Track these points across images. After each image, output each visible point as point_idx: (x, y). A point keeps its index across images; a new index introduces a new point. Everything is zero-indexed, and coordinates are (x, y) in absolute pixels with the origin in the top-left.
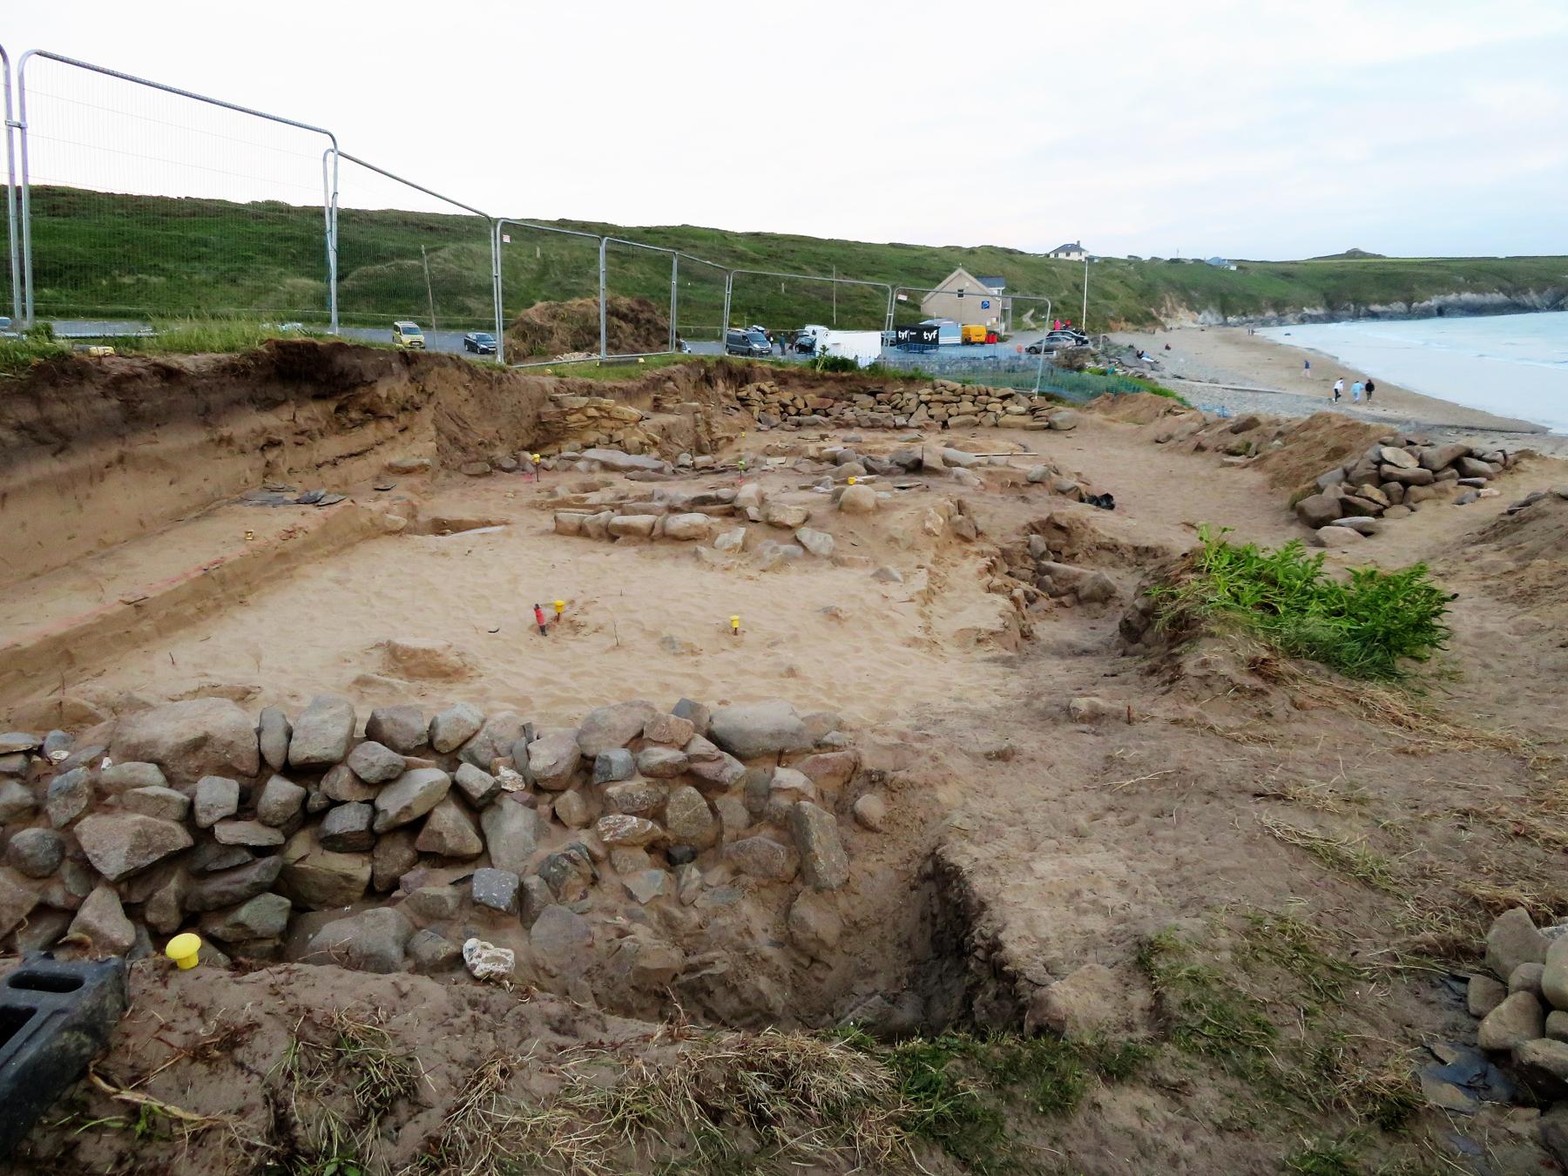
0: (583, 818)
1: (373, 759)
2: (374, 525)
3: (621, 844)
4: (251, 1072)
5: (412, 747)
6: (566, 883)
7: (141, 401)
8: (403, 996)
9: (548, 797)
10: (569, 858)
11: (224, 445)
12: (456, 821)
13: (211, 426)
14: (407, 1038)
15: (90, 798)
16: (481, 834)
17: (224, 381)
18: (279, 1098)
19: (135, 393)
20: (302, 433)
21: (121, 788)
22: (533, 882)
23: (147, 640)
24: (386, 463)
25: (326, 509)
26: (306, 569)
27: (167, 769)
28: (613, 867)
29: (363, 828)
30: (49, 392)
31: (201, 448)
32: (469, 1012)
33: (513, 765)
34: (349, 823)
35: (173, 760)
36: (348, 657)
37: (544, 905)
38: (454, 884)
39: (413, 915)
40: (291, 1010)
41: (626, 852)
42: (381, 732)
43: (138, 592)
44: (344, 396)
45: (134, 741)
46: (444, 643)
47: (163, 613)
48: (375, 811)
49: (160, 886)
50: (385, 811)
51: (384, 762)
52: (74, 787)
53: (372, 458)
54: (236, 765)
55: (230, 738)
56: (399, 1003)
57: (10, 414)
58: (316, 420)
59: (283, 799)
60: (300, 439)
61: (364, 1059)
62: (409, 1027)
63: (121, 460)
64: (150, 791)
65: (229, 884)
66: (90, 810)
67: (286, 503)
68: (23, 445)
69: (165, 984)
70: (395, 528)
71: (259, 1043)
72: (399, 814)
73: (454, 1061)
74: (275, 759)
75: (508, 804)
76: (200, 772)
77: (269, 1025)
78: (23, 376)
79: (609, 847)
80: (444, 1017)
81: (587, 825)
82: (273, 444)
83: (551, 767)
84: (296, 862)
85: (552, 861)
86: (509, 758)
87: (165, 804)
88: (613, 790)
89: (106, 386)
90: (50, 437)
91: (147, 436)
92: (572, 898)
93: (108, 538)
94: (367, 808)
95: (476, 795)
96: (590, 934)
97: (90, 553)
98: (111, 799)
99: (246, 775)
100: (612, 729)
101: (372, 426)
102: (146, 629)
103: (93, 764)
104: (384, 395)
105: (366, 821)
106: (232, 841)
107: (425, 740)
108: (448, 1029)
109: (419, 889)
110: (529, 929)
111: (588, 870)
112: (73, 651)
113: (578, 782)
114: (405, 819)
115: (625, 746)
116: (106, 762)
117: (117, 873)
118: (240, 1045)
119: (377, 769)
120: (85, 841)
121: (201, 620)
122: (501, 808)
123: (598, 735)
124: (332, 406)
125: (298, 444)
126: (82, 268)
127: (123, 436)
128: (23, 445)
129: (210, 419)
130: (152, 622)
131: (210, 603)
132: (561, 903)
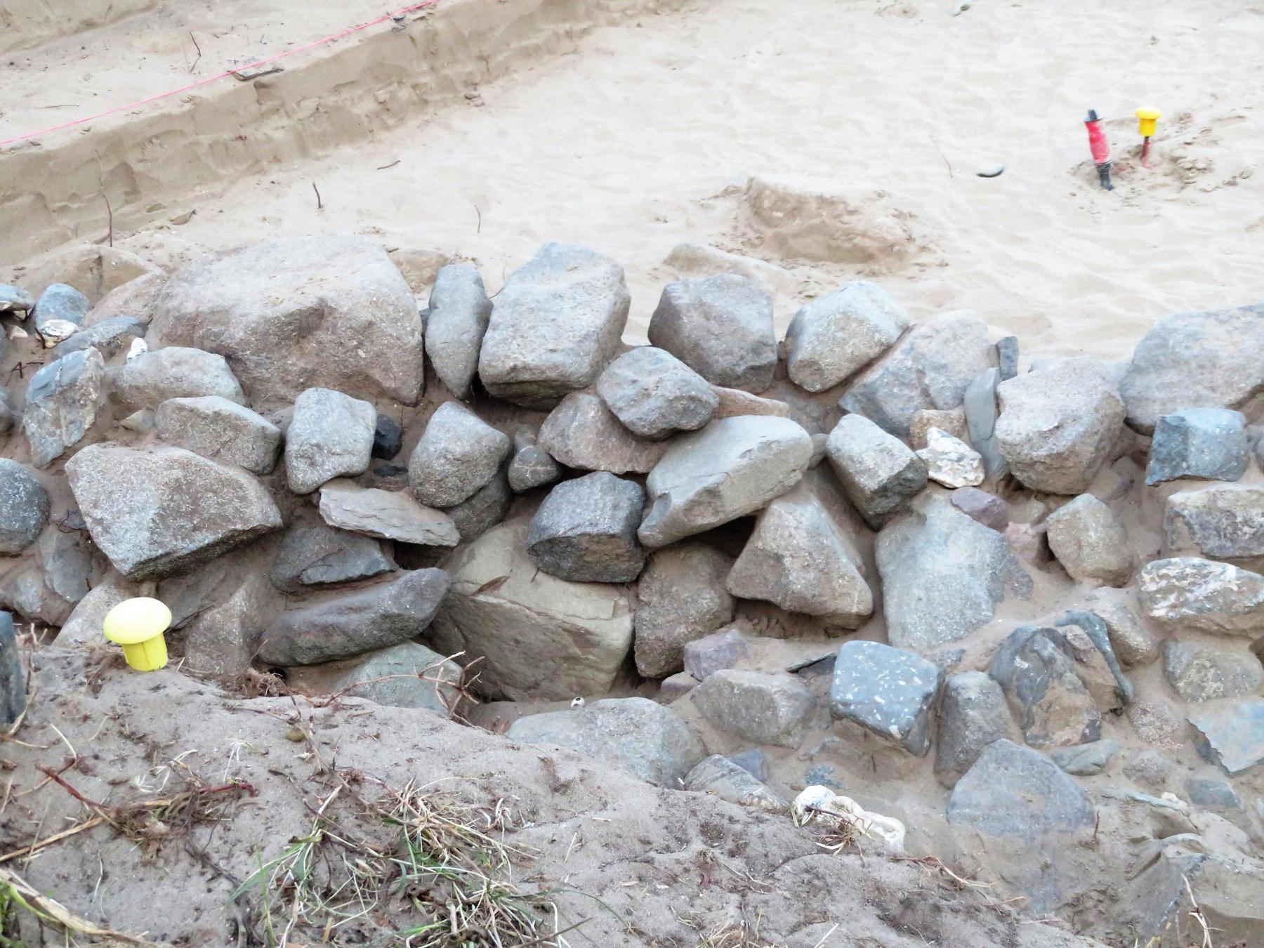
0: (1112, 562)
1: (649, 381)
3: (1192, 627)
4: (218, 874)
5: (740, 369)
6: (1049, 695)
8: (560, 788)
9: (1036, 507)
10: (1063, 643)
12: (814, 533)
14: (548, 872)
15: (100, 412)
16: (874, 576)
18: (259, 930)
21: (155, 396)
22: (971, 683)
23: (277, 159)
27: (246, 370)
28: (1170, 680)
29: (617, 528)
32: (698, 845)
33: (963, 429)
34: (588, 516)
35: (257, 352)
37: (989, 740)
38: (795, 671)
39: (703, 726)
40: (321, 773)
41: (1209, 648)
42: (677, 332)
43: (267, 58)
45: (189, 308)
46: (870, 187)
47: (310, 104)
48: (647, 499)
49: (213, 601)
50: (664, 497)
51: (669, 390)
52: (72, 385)
54: (377, 374)
55: (365, 316)
56: (546, 800)
59: (458, 449)
61: (444, 888)
62: (556, 849)
64: (205, 404)
65: (341, 612)
66: (98, 435)
69: (95, 690)
71: (246, 823)
72: (692, 505)
73: (640, 933)
74: (453, 370)
75: (939, 512)
76: (308, 380)
77: (271, 793)
79: (1165, 631)
80: (638, 847)
81: (1119, 578)
83: (1044, 436)
84: (481, 590)
85: (1021, 644)
86: (956, 413)
87: (230, 434)
88: (1187, 499)
92: (1061, 735)
94: (631, 490)
95: (869, 483)
96: (1094, 820)
98: (136, 417)
99: (395, 398)
100: (1209, 363)
102: (278, 135)
103: (113, 349)
105: (622, 514)
106: (351, 523)
107: (770, 357)
108: (642, 868)
109: (721, 673)
110: (950, 788)
111: (1105, 677)
112: (138, 167)
113: (1112, 479)
114: (707, 519)
115: (1238, 406)
116: (138, 345)
117: (134, 558)
118: (209, 821)
119: (654, 403)
120: (82, 492)
121: (387, 128)
122: (922, 519)
123: (1171, 376)
130: (285, 122)
131: (405, 94)
132: (1033, 743)
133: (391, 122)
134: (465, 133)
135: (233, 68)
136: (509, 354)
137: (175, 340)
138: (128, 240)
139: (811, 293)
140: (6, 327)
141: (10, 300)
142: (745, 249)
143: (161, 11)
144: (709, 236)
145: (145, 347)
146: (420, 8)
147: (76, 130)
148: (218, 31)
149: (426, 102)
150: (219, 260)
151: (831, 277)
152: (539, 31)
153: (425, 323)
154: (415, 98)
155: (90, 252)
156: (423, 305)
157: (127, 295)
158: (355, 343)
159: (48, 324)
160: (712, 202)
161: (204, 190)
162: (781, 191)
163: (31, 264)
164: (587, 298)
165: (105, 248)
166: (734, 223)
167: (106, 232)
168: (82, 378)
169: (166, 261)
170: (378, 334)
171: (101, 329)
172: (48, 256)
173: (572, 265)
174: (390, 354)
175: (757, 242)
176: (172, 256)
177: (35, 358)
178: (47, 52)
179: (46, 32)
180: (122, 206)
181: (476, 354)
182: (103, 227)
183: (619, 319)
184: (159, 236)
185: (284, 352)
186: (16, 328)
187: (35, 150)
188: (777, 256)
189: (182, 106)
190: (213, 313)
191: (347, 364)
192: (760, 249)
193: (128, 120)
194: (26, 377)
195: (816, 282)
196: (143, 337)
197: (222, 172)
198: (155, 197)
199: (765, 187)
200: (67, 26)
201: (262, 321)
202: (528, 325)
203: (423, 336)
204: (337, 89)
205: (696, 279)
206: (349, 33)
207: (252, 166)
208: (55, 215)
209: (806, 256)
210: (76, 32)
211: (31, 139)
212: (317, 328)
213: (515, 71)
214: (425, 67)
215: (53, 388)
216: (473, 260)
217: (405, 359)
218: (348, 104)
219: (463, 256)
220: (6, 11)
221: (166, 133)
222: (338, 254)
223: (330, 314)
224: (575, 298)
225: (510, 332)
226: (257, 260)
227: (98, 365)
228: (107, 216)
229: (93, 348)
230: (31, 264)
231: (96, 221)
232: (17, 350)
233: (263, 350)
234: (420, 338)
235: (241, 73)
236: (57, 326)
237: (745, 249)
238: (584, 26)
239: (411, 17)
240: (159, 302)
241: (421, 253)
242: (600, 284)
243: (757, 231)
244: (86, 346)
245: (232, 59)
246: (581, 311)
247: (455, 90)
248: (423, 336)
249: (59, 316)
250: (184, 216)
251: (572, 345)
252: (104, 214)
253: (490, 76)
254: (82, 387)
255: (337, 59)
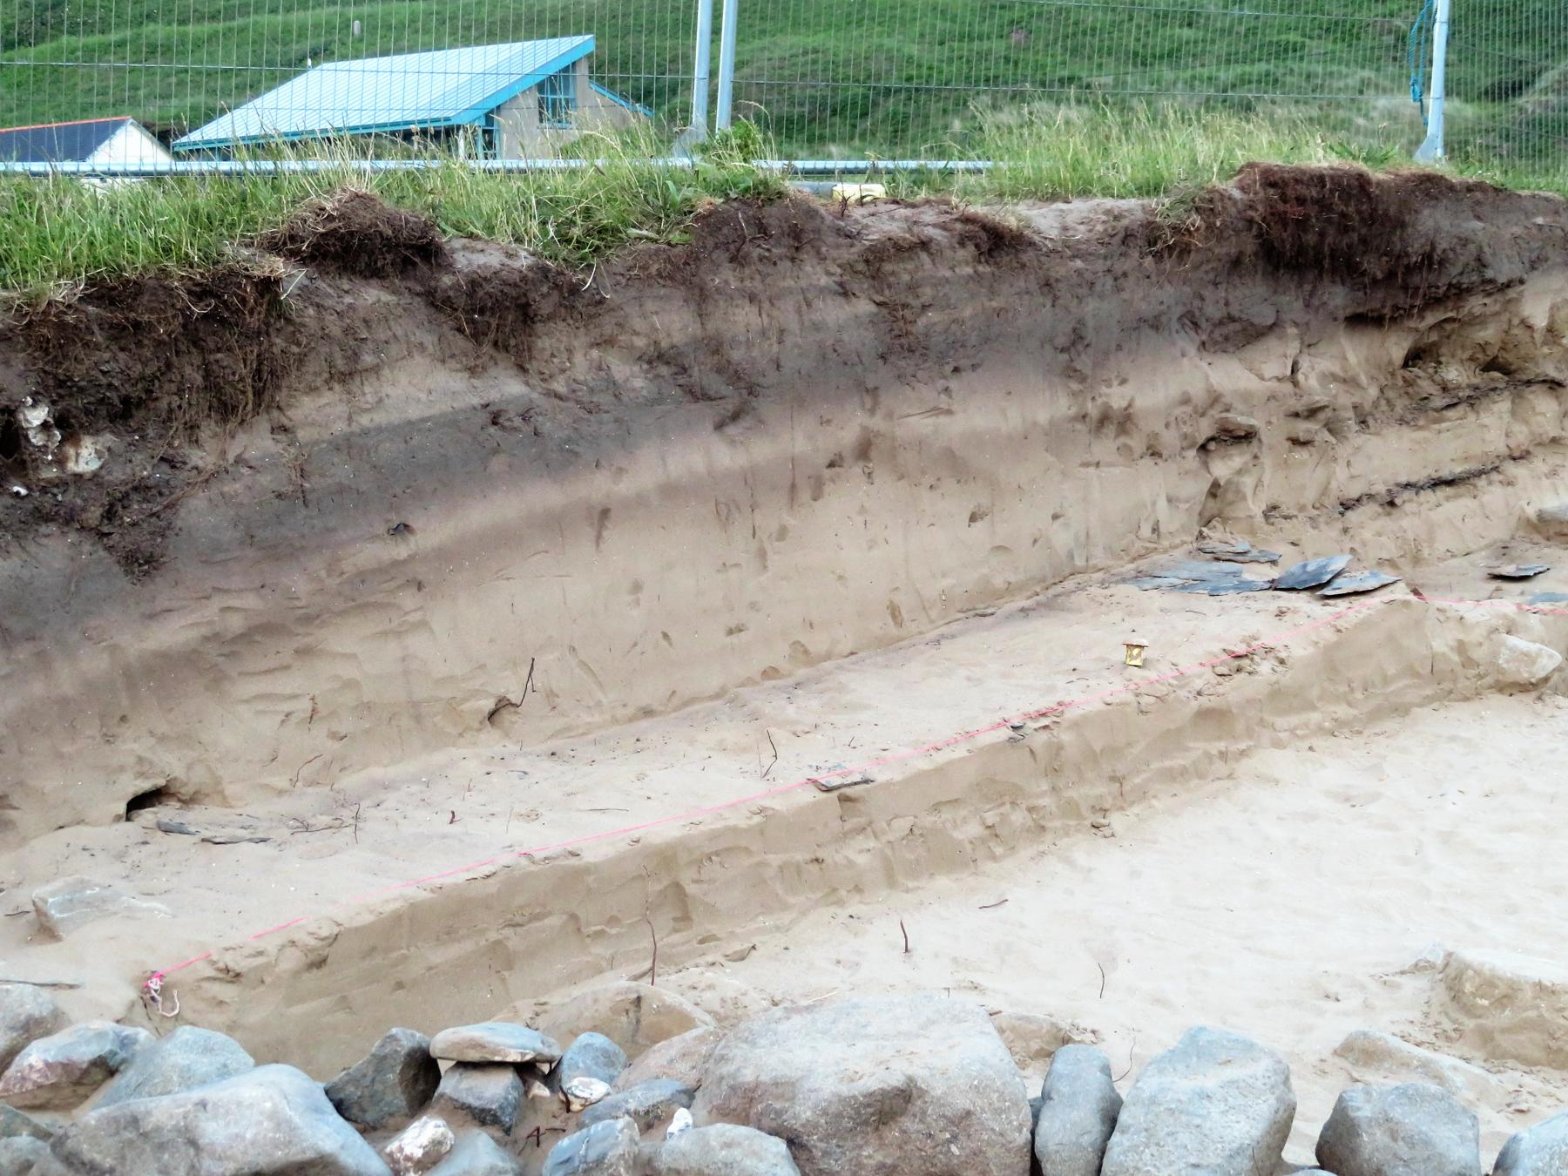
2: (1468, 662)
7: (925, 307)
11: (1111, 429)
13: (1083, 380)
17: (1127, 265)
19: (912, 288)
20: (1312, 413)
23: (858, 889)
24: (1531, 512)
25: (1342, 604)
26: (1272, 761)
27: (811, 1160)
30: (725, 277)
31: (1055, 437)
36: (1334, 988)
42: (1354, 1151)
43: (856, 766)
44: (1431, 318)
45: (748, 1076)
47: (902, 825)
53: (1492, 494)
55: (962, 1103)
57: (638, 323)
58: (1350, 382)
60: (1302, 428)
63: (864, 451)
67: (1244, 587)
68: (658, 400)
70: (1525, 676)
78: (675, 237)
82: (1235, 437)
89: (849, 267)
90: (715, 384)
91: (928, 394)
93: (817, 643)
97: (770, 673)
101: (1503, 405)
102: (862, 860)
103: (651, 1120)
104: (1540, 321)
112: (691, 889)
116: (682, 1117)
121: (994, 858)
124: (1396, 346)
125: (1295, 442)
126: (913, 94)
127: (874, 392)
128: (658, 400)
129: (1084, 363)
130: (872, 844)
131: (1018, 817)
133: (999, 850)
134: (1090, 870)
135: (815, 776)
136: (1140, 1165)
137: (727, 1115)
138: (673, 977)
139: (1524, 1107)
140: (524, 1082)
141: (534, 1050)
142: (1438, 1043)
143: (731, 701)
144: (1393, 1022)
145: (690, 1121)
146: (1043, 715)
147: (623, 840)
148: (799, 728)
149: (1043, 828)
150: (788, 1018)
151: (1550, 1088)
152: (1187, 749)
153: (1036, 1117)
154: (1030, 823)
155: (629, 990)
156: (1034, 1092)
157: (673, 1052)
158: (948, 1136)
159: (575, 1082)
160: (1398, 979)
161: (769, 922)
162: (1487, 972)
163: (555, 999)
164: (1241, 1101)
165: (644, 986)
166: (1425, 1009)
167: (647, 965)
168: (612, 1155)
169: (717, 1007)
170: (977, 1127)
171: (639, 1094)
172: (576, 991)
173: (1224, 1057)
174: (990, 1154)
175: (1453, 1035)
176: (723, 1001)
177: (557, 1124)
178: (595, 742)
179: (597, 718)
180: (669, 935)
181: (1097, 1162)
182: (645, 959)
183: (1281, 1130)
184: (710, 975)
185: (859, 1141)
186: (538, 1083)
187: (573, 861)
188: (1479, 1055)
189: (750, 818)
190: (776, 1084)
191: (935, 1161)
192: (1457, 1045)
193: (685, 831)
194: (543, 1145)
195: (1530, 1093)
196: (688, 1107)
197: (792, 900)
198: (709, 927)
199: (1468, 966)
200: (621, 713)
201: (835, 1099)
202: (1166, 1130)
203: (1033, 1133)
204: (937, 807)
205: (1379, 1080)
206: (956, 741)
207: (828, 895)
208: (588, 941)
209: (1516, 1058)
210: (631, 720)
211: (570, 849)
212: (903, 1113)
213: (1154, 797)
214: (1045, 786)
215: (577, 1163)
216: (1093, 1032)
217: (1008, 1161)
218: (949, 825)
219: (1081, 1026)
220: (551, 691)
221: (729, 850)
222: (934, 1022)
223: (920, 1097)
224: (1226, 1100)
225: (1142, 1138)
226: (834, 1022)
227: (632, 1140)
228: (650, 946)
229: (627, 1117)
230: (555, 999)
231: (637, 951)
232: (536, 1112)
233: (834, 1136)
234: (1029, 1136)
235: (823, 782)
236: (587, 1086)
237: (1438, 1043)
238: (1242, 746)
239: (1032, 725)
240: (710, 1065)
241: (1028, 1019)
242: (1259, 1084)
243: (1454, 1022)
244: (620, 1114)
245: (814, 764)
246: (1234, 1118)
247: (1079, 816)
248: (1033, 1133)
249: (589, 1073)
250: (742, 951)
251: (1219, 1161)
252: (646, 943)
253: (1123, 801)
254: (611, 1165)
255: (940, 771)
